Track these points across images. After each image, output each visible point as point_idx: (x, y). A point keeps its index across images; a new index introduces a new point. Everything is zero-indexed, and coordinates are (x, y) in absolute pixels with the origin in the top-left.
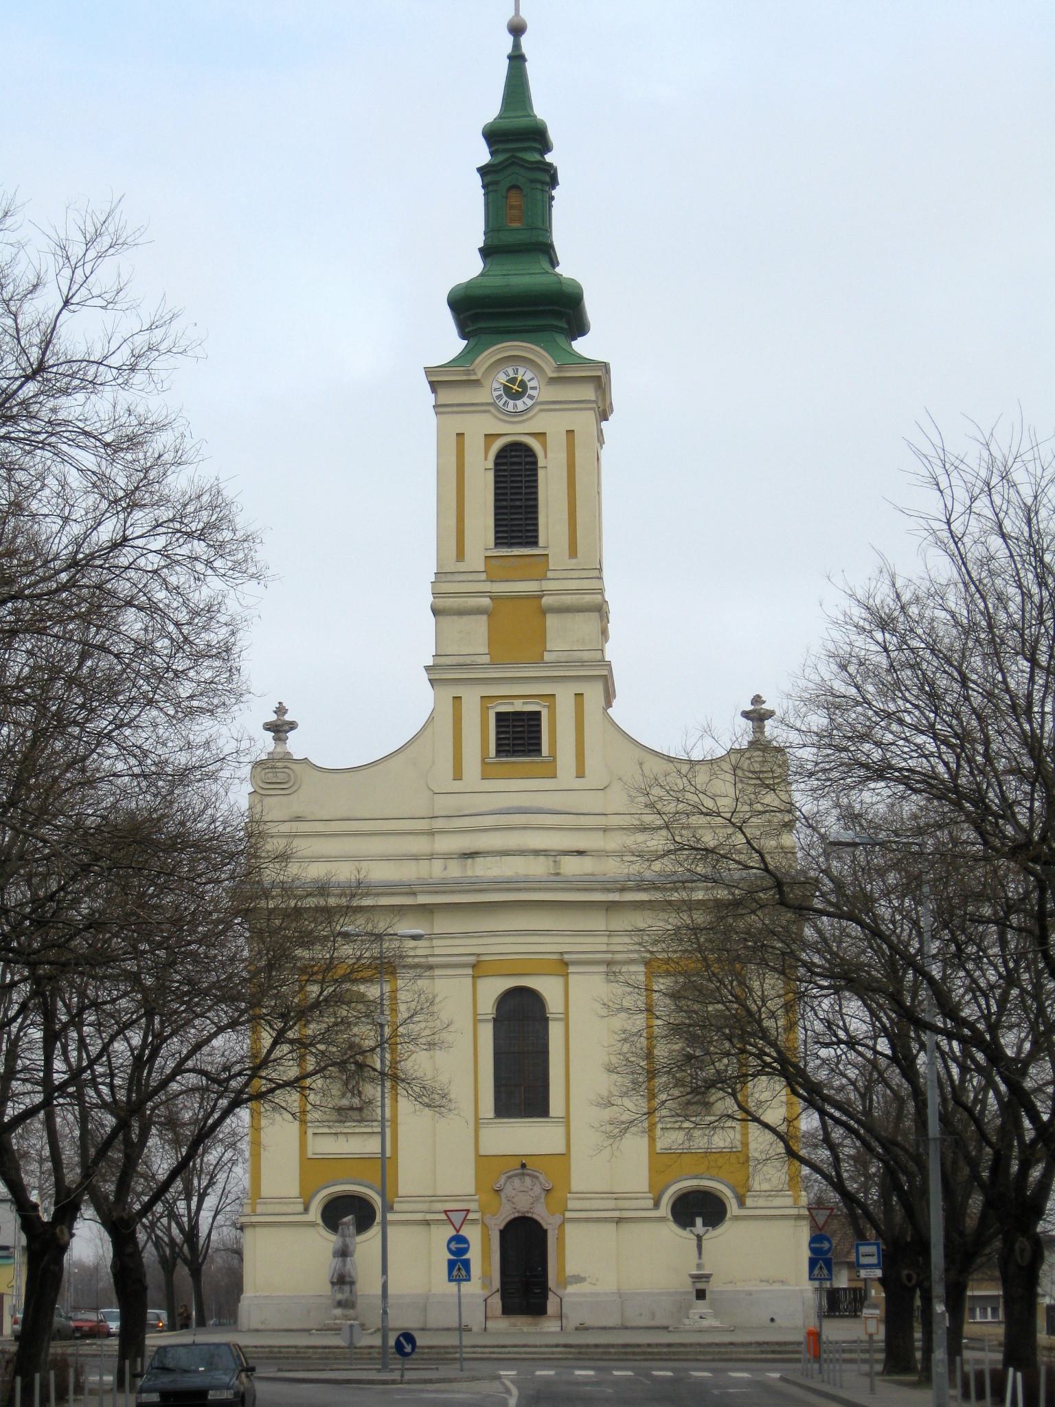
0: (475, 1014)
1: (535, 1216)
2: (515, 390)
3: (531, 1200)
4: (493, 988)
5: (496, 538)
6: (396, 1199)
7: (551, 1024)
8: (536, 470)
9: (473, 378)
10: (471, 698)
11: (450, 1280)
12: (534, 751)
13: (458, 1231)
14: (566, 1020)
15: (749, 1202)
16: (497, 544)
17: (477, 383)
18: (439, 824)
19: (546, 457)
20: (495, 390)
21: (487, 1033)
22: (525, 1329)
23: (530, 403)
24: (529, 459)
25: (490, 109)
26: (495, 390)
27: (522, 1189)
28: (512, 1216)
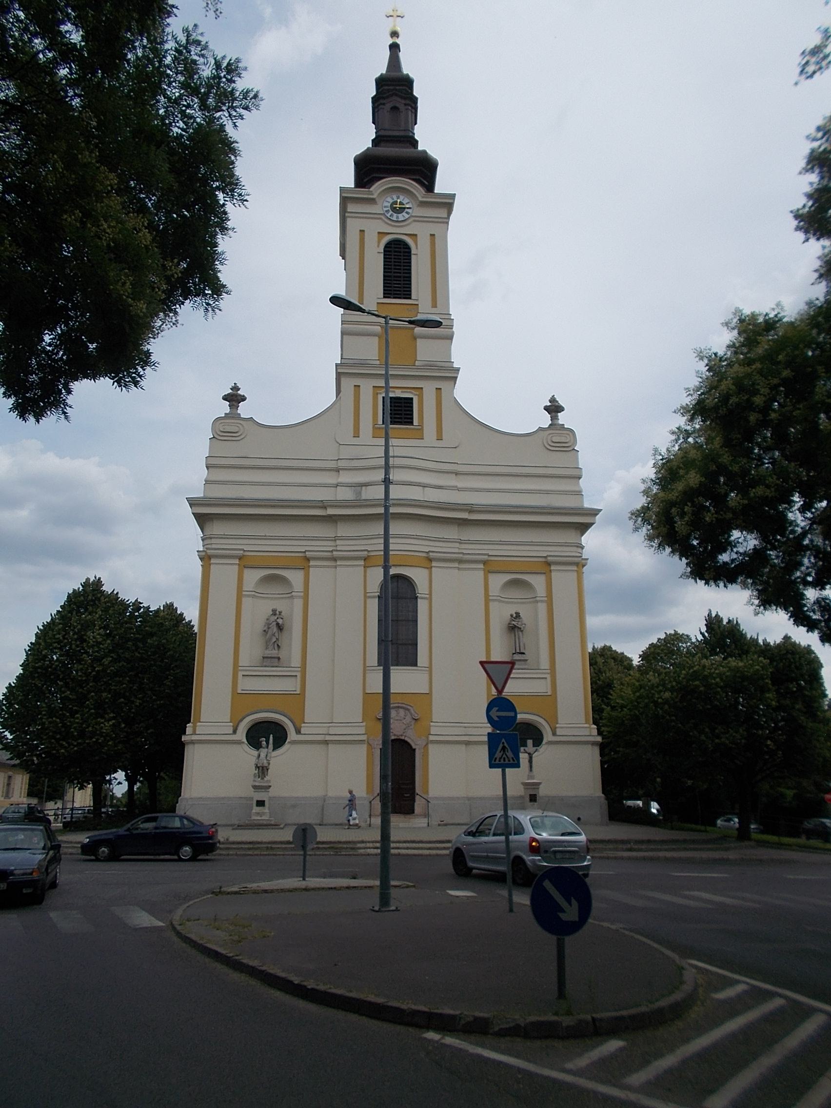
2: (398, 209)
3: (404, 727)
5: (384, 294)
6: (303, 725)
7: (419, 601)
8: (410, 256)
9: (371, 197)
10: (367, 387)
11: (492, 766)
12: (408, 422)
13: (500, 692)
15: (558, 732)
16: (384, 297)
17: (372, 201)
18: (341, 464)
19: (417, 248)
20: (385, 207)
21: (373, 606)
22: (401, 825)
23: (407, 216)
24: (407, 250)
25: (382, 69)
26: (385, 207)
27: (397, 718)
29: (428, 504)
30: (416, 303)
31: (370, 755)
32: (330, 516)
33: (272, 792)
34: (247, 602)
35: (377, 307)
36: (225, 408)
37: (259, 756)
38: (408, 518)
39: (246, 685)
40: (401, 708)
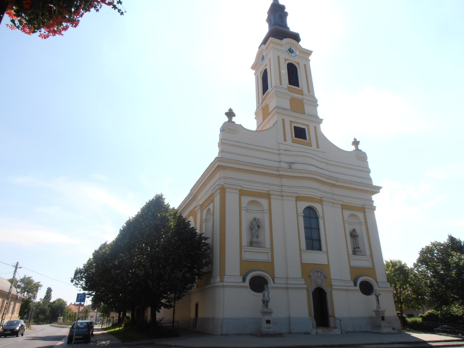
0: (297, 214)
1: (323, 287)
4: (303, 205)
14: (324, 219)
15: (276, 281)
17: (281, 45)
21: (301, 220)
28: (316, 287)
29: (323, 175)
30: (302, 89)
31: (308, 295)
32: (280, 175)
33: (273, 315)
34: (244, 213)
35: (287, 88)
36: (226, 119)
37: (264, 295)
38: (313, 180)
39: (247, 256)
40: (320, 272)
